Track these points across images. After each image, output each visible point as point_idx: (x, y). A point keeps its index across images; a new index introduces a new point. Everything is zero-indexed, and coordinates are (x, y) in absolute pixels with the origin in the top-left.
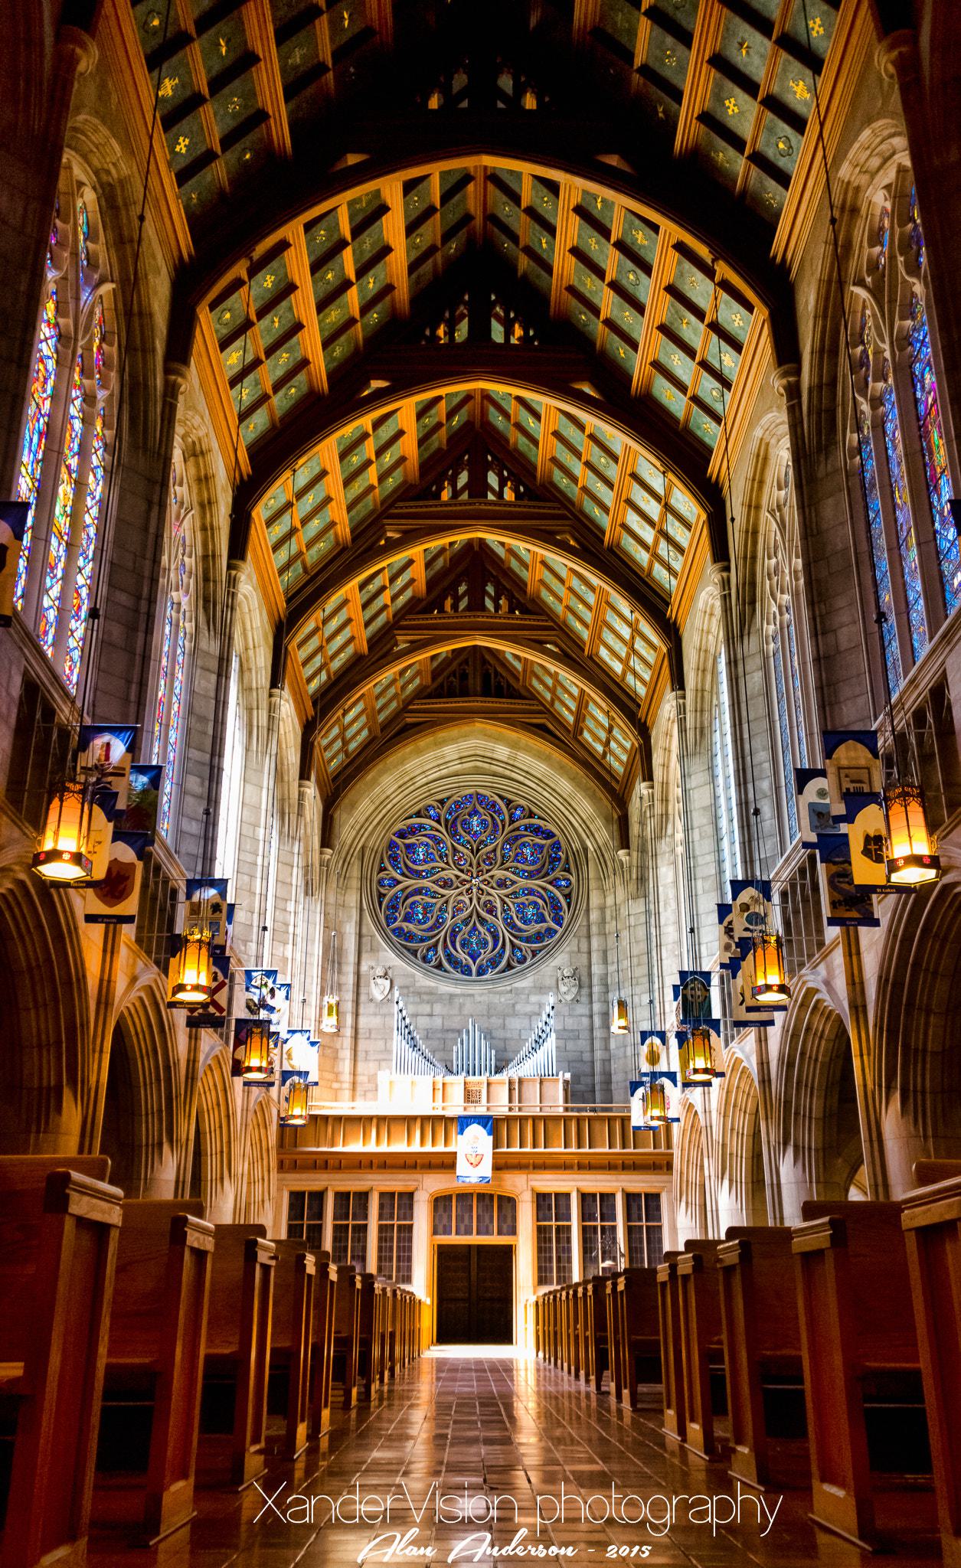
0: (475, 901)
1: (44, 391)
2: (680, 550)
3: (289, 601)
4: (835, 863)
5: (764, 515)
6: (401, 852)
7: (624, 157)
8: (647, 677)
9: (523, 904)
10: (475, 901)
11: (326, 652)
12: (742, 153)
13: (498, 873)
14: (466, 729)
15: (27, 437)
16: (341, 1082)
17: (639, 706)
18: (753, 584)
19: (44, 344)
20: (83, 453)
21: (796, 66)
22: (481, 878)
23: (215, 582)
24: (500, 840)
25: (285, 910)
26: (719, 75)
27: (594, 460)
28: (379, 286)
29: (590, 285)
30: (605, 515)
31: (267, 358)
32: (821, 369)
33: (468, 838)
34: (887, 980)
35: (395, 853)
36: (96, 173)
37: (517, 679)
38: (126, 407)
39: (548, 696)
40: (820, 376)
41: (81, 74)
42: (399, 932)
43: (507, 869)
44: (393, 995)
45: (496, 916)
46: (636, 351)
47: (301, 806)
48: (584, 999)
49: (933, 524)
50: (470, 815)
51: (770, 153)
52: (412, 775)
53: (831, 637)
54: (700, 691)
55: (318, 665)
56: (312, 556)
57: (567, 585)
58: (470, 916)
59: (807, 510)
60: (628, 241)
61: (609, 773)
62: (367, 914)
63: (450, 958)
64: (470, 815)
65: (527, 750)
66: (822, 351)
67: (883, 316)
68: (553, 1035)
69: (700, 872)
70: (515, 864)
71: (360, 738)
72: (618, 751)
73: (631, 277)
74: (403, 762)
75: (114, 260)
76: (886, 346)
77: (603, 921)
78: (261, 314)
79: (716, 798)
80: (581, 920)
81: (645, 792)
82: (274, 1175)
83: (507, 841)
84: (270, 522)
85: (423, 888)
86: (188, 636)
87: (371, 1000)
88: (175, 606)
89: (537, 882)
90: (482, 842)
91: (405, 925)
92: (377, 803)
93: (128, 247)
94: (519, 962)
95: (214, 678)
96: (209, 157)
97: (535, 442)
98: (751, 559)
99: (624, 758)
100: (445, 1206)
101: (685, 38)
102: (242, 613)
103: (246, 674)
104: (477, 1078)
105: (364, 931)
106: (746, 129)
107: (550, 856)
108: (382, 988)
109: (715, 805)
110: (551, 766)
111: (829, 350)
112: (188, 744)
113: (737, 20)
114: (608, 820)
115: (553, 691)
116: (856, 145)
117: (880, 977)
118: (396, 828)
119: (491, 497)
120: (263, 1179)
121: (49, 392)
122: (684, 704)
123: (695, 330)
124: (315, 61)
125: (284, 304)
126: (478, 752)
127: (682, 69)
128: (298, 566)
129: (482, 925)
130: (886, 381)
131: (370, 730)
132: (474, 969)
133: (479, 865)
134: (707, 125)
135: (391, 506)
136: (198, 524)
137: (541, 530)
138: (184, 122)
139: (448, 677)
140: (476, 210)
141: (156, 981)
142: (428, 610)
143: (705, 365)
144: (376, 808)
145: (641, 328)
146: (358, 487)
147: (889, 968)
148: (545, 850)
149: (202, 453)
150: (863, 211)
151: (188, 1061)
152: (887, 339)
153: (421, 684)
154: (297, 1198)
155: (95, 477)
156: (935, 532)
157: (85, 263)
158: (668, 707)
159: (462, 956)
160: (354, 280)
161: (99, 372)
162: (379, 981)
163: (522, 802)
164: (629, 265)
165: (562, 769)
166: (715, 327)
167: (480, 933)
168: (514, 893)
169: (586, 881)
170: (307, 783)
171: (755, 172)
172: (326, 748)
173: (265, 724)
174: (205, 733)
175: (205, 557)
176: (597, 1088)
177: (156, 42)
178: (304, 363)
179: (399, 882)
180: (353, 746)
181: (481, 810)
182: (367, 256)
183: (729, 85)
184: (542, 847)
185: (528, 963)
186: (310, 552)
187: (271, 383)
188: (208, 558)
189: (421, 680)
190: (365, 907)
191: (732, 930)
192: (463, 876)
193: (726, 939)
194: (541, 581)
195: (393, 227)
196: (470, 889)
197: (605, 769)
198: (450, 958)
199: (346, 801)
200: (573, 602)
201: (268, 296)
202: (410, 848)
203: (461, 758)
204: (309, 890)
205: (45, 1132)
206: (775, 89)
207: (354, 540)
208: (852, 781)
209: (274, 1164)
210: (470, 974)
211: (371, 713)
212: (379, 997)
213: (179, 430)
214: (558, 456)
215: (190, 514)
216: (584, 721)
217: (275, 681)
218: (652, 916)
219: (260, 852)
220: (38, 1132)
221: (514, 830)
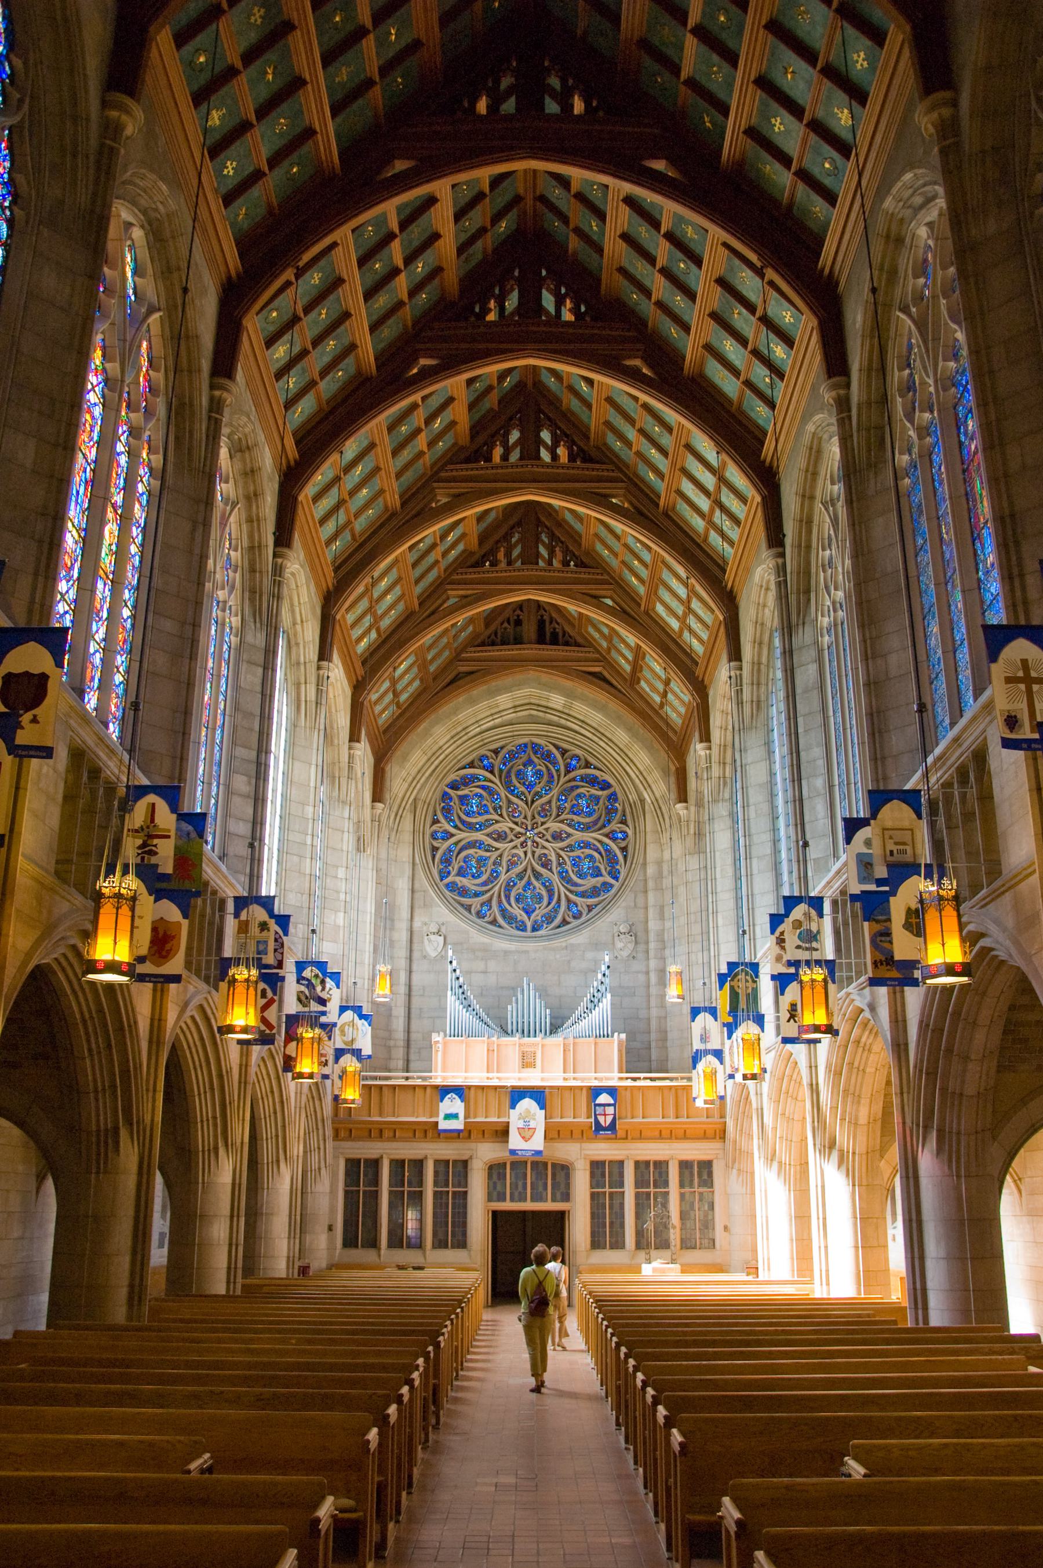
0: (529, 855)
1: (91, 439)
2: (731, 543)
3: (336, 569)
4: (877, 921)
5: (818, 506)
6: (455, 804)
7: (672, 161)
8: (705, 636)
9: (579, 857)
10: (529, 855)
11: (375, 611)
12: (789, 168)
13: (554, 826)
14: (519, 677)
15: (74, 492)
16: (396, 1040)
17: (697, 664)
18: (808, 573)
19: (92, 393)
20: (129, 488)
21: (841, 96)
22: (536, 831)
23: (261, 572)
24: (555, 791)
25: (336, 877)
26: (764, 95)
27: (648, 428)
28: (427, 269)
29: (640, 268)
30: (659, 481)
31: (314, 348)
32: (869, 385)
33: (522, 789)
34: (928, 1025)
35: (448, 804)
36: (144, 212)
37: (573, 626)
38: (172, 428)
39: (605, 644)
40: (869, 393)
41: (128, 138)
42: (452, 887)
43: (562, 822)
44: (447, 952)
45: (551, 870)
46: (689, 334)
47: (350, 768)
48: (640, 956)
49: (977, 573)
50: (525, 765)
51: (816, 172)
52: (465, 725)
53: (879, 661)
54: (757, 664)
55: (367, 624)
56: (360, 525)
57: (622, 542)
58: (525, 870)
59: (857, 527)
60: (678, 233)
61: (668, 724)
62: (419, 868)
63: (503, 912)
64: (525, 765)
65: (583, 699)
66: (870, 369)
67: (927, 351)
68: (609, 996)
69: (756, 851)
70: (570, 816)
71: (411, 689)
72: (676, 703)
73: (682, 266)
74: (455, 712)
75: (161, 288)
76: (931, 381)
77: (660, 876)
78: (308, 309)
79: (772, 774)
80: (638, 874)
81: (702, 753)
82: (330, 1144)
83: (562, 793)
84: (317, 498)
85: (476, 841)
86: (234, 631)
87: (425, 957)
88: (221, 605)
89: (594, 835)
90: (537, 794)
91: (458, 879)
92: (430, 754)
93: (176, 275)
94: (575, 917)
95: (260, 670)
96: (257, 176)
97: (589, 406)
98: (805, 548)
99: (683, 710)
100: (499, 1174)
101: (731, 58)
102: (289, 589)
103: (294, 650)
104: (532, 1040)
105: (417, 886)
106: (792, 147)
107: (607, 808)
108: (435, 944)
109: (772, 783)
110: (607, 715)
111: (879, 368)
112: (234, 743)
113: (782, 47)
114: (666, 773)
115: (610, 640)
116: (900, 184)
117: (921, 1022)
118: (448, 780)
119: (541, 563)
120: (319, 1148)
121: (96, 438)
122: (741, 675)
123: (746, 320)
124: (362, 76)
125: (332, 297)
126: (533, 701)
127: (730, 85)
128: (347, 535)
129: (537, 879)
130: (932, 412)
131: (421, 680)
132: (529, 925)
133: (534, 817)
134: (752, 139)
135: (442, 469)
136: (244, 517)
137: (595, 493)
138: (233, 147)
139: (502, 624)
140: (526, 190)
141: (206, 999)
142: (479, 564)
143: (756, 353)
144: (429, 759)
145: (695, 314)
146: (406, 455)
147: (929, 1015)
148: (601, 802)
149: (248, 448)
150: (908, 240)
151: (241, 1065)
152: (931, 375)
153: (474, 631)
154: (353, 1166)
155: (141, 505)
156: (979, 580)
157: (133, 298)
158: (723, 672)
159: (517, 911)
160: (403, 268)
161: (146, 400)
162: (432, 937)
163: (578, 752)
164: (679, 255)
165: (618, 719)
166: (766, 321)
167: (535, 888)
168: (570, 846)
169: (643, 834)
170: (357, 745)
171: (801, 187)
172: (376, 702)
173: (314, 699)
174: (252, 730)
175: (251, 548)
176: (653, 1044)
177: (203, 78)
178: (352, 347)
179: (452, 835)
180: (403, 697)
181: (536, 760)
182: (416, 243)
183: (774, 105)
184: (597, 799)
185: (583, 919)
186: (359, 520)
187: (318, 370)
188: (254, 549)
189: (474, 628)
190: (417, 860)
191: (783, 941)
192: (518, 829)
193: (777, 950)
194: (596, 535)
195: (442, 218)
196: (525, 842)
197: (662, 717)
198: (503, 912)
199: (398, 753)
200: (628, 557)
201: (315, 293)
202: (463, 799)
203: (515, 707)
204: (360, 846)
205: (105, 1172)
206: (820, 114)
207: (403, 504)
208: (896, 843)
209: (329, 1132)
210: (524, 930)
211: (422, 664)
212: (433, 954)
213: (225, 431)
214: (611, 420)
215: (236, 509)
216: (641, 671)
217: (324, 655)
218: (707, 870)
219: (310, 832)
220: (98, 1173)
221: (570, 781)
